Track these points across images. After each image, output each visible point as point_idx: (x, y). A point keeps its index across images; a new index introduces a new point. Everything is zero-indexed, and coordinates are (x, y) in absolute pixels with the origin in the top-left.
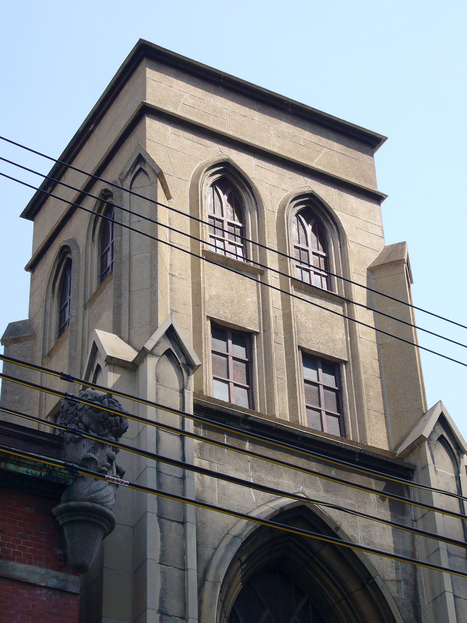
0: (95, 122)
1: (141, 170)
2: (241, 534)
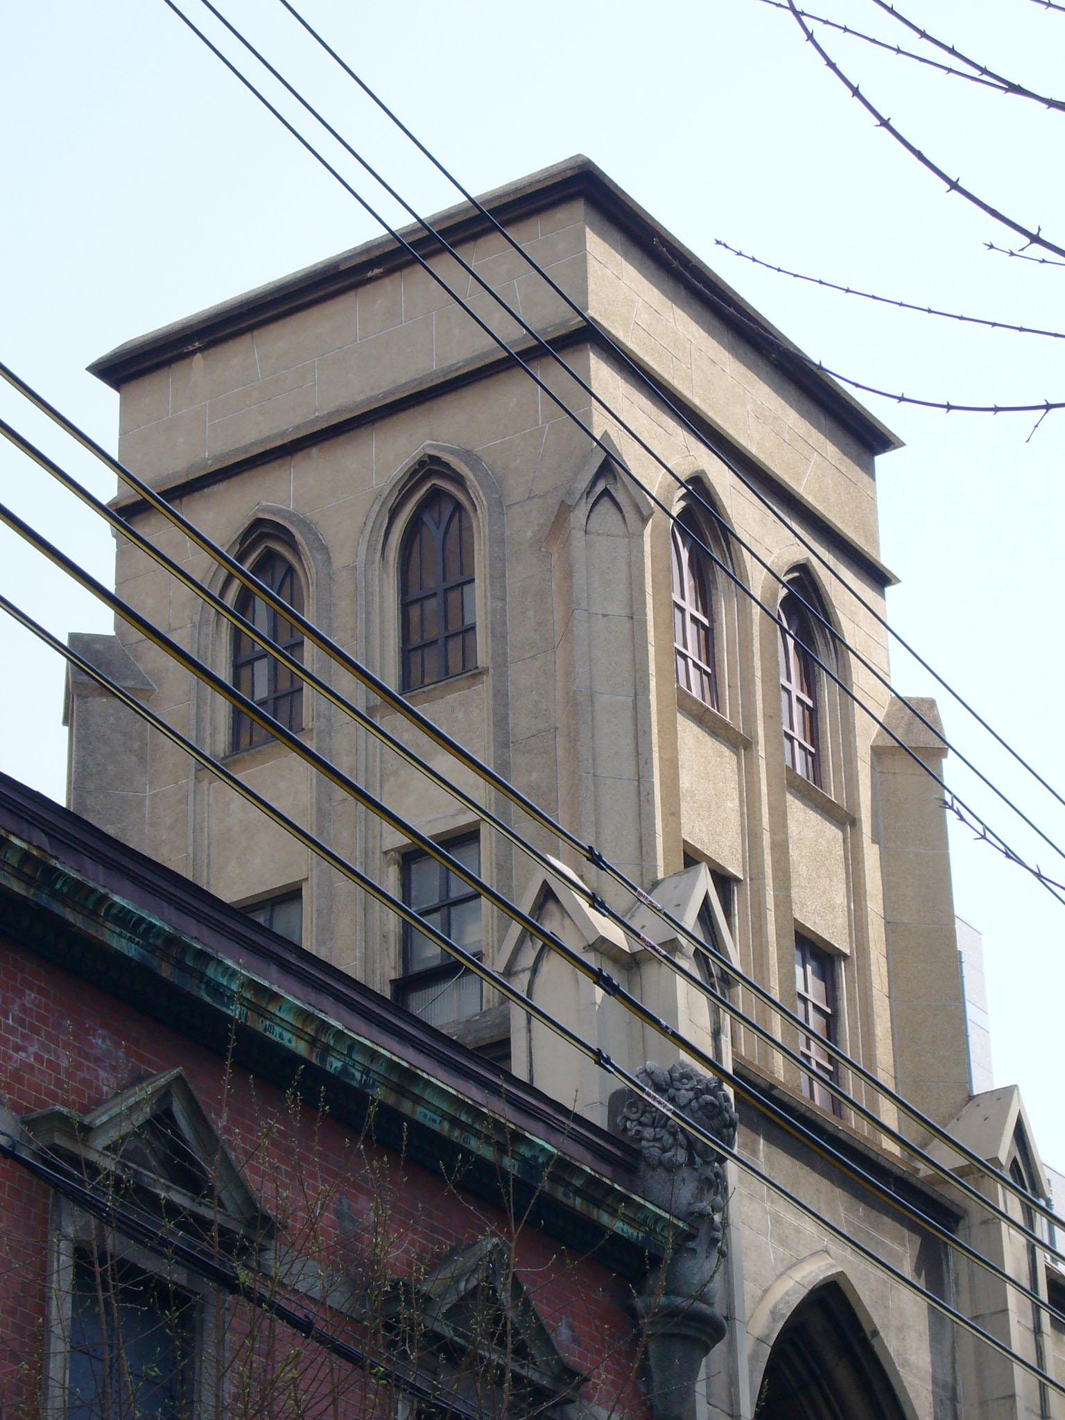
0: (388, 266)
1: (606, 493)
2: (768, 1336)
